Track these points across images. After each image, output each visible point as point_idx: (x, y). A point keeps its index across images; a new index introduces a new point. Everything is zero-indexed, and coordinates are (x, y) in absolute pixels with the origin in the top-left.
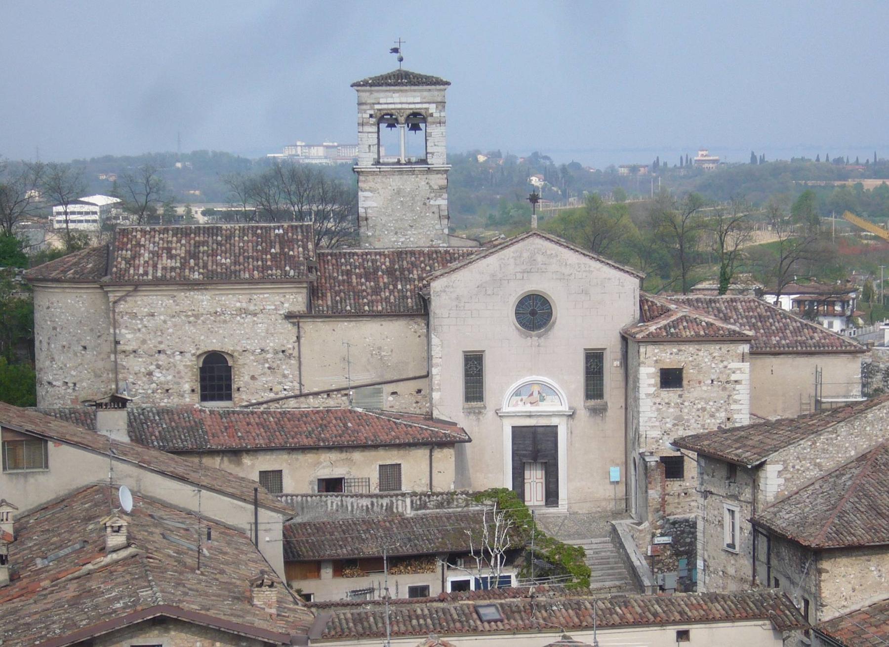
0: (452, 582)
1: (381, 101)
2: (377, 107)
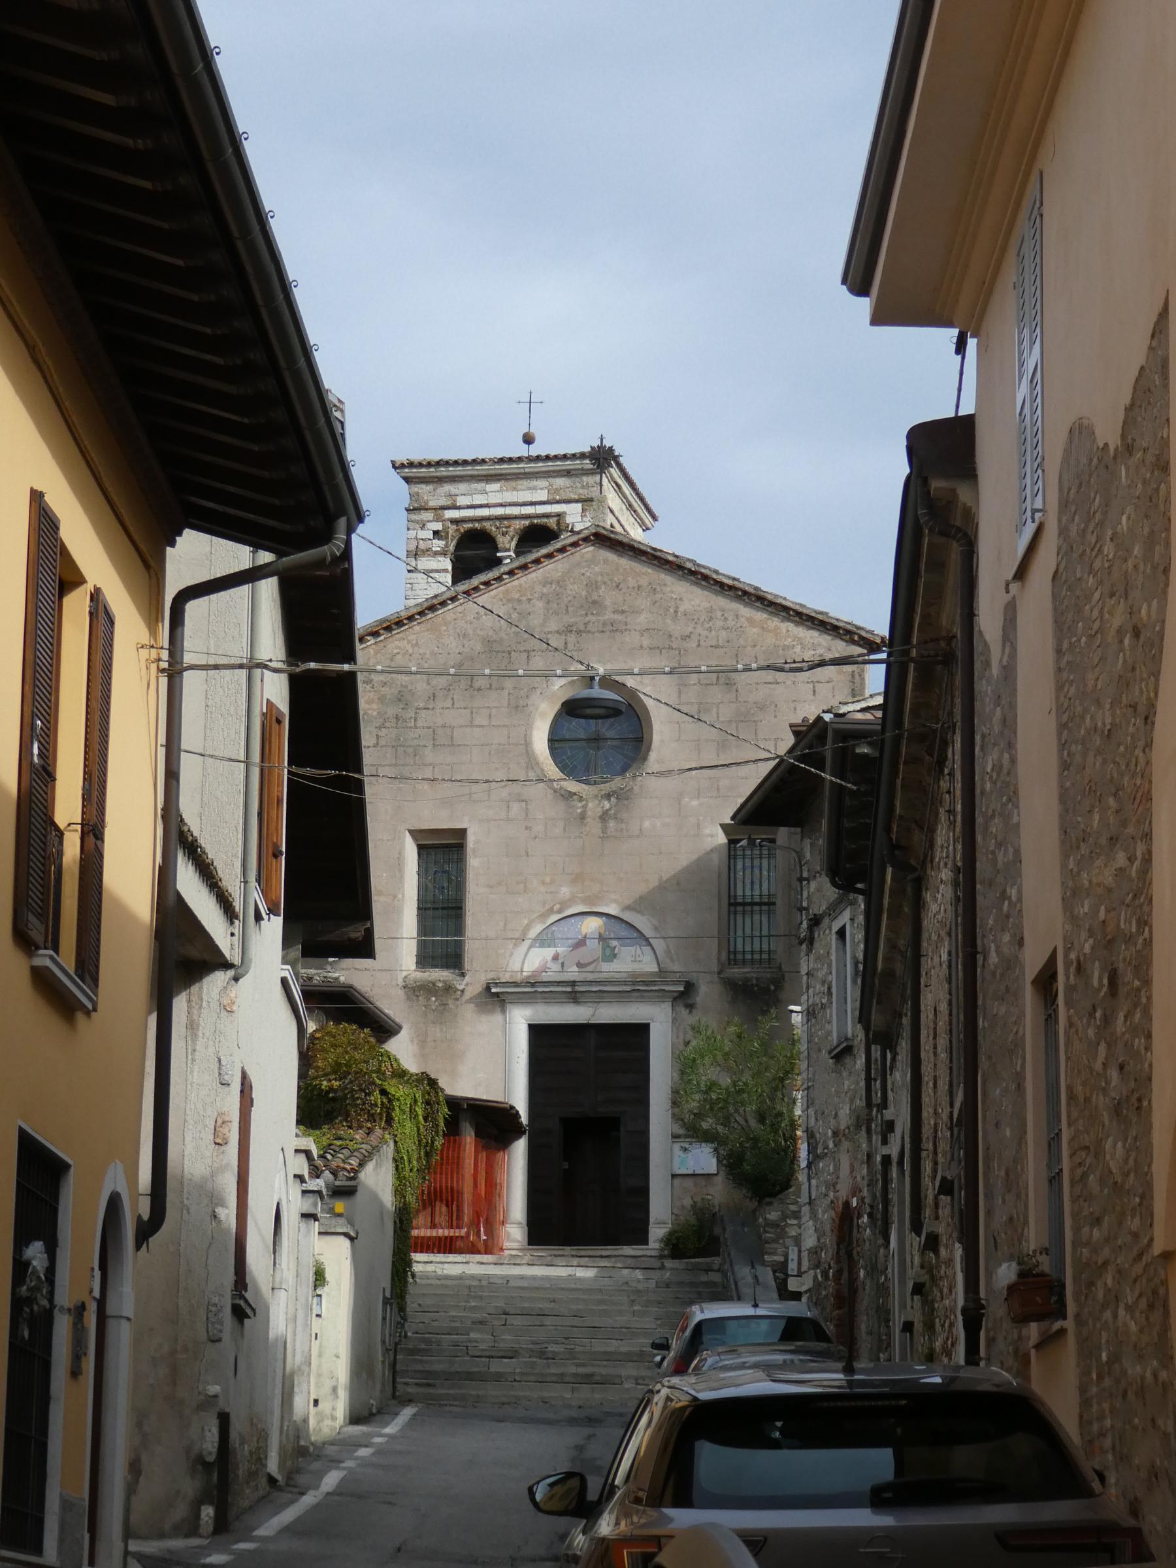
0: (641, 1031)
1: (462, 501)
2: (449, 514)
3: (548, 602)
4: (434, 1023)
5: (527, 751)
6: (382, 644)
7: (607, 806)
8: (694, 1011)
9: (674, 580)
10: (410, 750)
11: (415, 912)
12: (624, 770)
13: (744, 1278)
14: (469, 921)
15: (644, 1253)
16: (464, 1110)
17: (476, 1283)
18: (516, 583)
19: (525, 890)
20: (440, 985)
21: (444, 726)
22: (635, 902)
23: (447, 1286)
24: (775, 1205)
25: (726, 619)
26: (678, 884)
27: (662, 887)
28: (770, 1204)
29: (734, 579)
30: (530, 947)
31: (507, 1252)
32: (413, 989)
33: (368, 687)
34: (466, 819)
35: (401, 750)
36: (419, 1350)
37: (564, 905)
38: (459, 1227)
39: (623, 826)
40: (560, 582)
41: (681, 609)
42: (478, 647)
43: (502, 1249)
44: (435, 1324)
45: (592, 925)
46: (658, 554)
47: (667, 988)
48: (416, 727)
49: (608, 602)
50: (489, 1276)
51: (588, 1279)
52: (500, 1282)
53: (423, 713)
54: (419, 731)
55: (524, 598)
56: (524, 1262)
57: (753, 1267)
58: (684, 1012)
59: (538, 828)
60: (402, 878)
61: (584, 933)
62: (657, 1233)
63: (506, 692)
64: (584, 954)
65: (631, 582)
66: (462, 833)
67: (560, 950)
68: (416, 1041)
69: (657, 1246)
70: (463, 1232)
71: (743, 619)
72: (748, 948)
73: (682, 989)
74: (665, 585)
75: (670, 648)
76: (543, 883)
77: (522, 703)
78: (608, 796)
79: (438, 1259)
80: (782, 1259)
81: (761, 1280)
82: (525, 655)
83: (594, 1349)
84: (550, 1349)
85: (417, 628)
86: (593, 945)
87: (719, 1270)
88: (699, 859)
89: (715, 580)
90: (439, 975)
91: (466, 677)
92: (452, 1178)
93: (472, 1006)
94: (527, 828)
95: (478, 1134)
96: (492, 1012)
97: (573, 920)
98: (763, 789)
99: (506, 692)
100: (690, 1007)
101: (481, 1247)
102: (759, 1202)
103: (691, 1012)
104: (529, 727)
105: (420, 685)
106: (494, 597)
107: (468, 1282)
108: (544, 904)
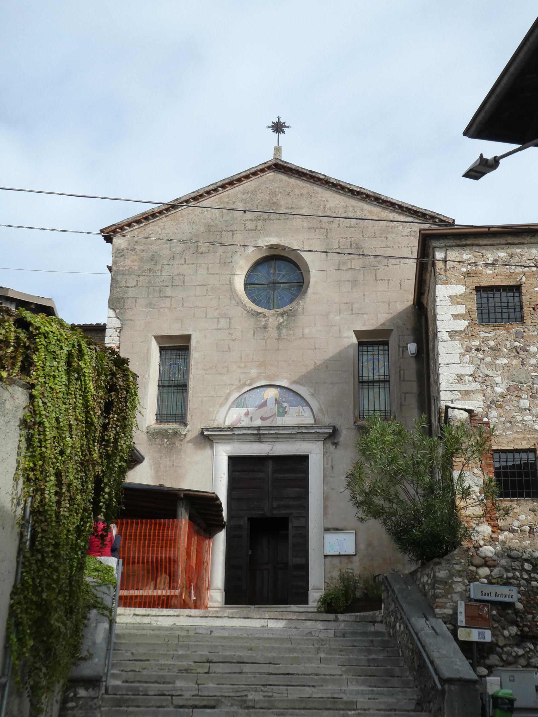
0: (304, 459)
3: (246, 203)
4: (166, 456)
5: (231, 289)
6: (143, 228)
7: (281, 320)
8: (338, 447)
9: (323, 191)
10: (157, 289)
11: (157, 388)
12: (291, 301)
13: (422, 629)
14: (191, 391)
15: (305, 610)
16: (181, 499)
17: (184, 633)
18: (226, 193)
19: (228, 372)
20: (171, 431)
21: (178, 275)
22: (299, 378)
23: (158, 636)
24: (444, 564)
25: (355, 212)
26: (327, 367)
27: (317, 369)
28: (439, 563)
29: (361, 188)
30: (230, 407)
31: (210, 609)
32: (153, 434)
33: (133, 253)
34: (191, 329)
35: (151, 288)
36: (127, 700)
37: (253, 381)
38: (175, 588)
39: (292, 332)
40: (254, 192)
41: (328, 206)
42: (202, 229)
43: (207, 608)
44: (145, 672)
45: (271, 394)
46: (314, 174)
47: (321, 431)
48: (162, 276)
49: (282, 203)
50: (195, 627)
51: (277, 630)
52: (204, 632)
53: (166, 267)
54: (163, 278)
55: (231, 202)
56: (226, 615)
57: (427, 619)
58: (332, 448)
59: (237, 334)
60: (148, 365)
61: (265, 398)
62: (315, 596)
63: (218, 255)
64: (264, 412)
65: (297, 192)
66: (188, 338)
67: (250, 409)
68: (153, 467)
69: (315, 604)
70: (177, 592)
71: (366, 212)
72: (371, 408)
73: (331, 431)
74: (317, 193)
75: (321, 228)
76: (240, 367)
77: (228, 260)
78: (282, 315)
79: (163, 613)
80: (450, 612)
81: (438, 631)
82: (231, 233)
83: (290, 697)
84: (250, 697)
85: (164, 219)
86: (271, 405)
87: (381, 622)
88: (341, 352)
89: (348, 189)
90: (171, 426)
91: (192, 246)
92: (170, 550)
93: (191, 444)
94: (230, 334)
95: (191, 518)
96: (204, 448)
97: (258, 390)
98: (508, 74)
99: (218, 255)
100: (336, 444)
101: (192, 604)
102: (423, 564)
103: (336, 447)
104: (232, 274)
105: (165, 252)
106: (212, 201)
107: (177, 633)
108: (240, 380)
